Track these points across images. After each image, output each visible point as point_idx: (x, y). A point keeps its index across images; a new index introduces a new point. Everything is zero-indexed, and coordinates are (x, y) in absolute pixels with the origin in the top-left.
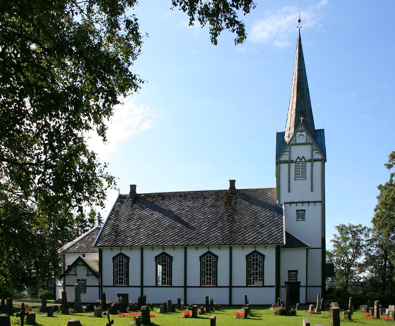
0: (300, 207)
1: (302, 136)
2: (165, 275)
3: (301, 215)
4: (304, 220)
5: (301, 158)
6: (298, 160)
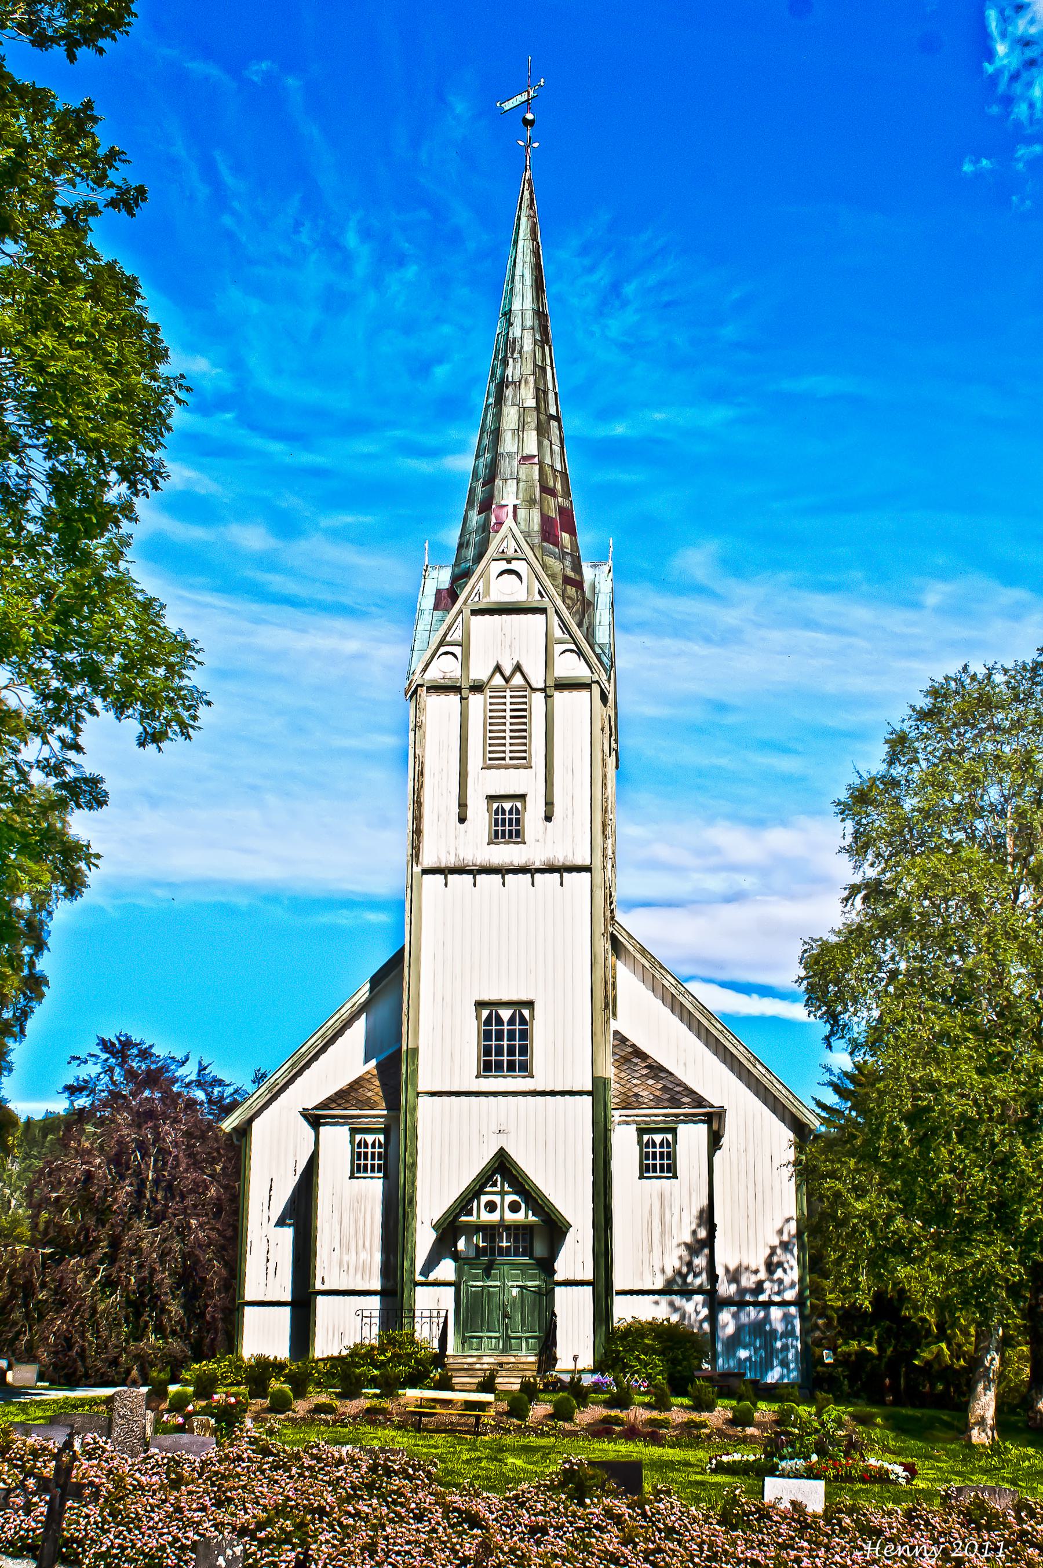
0: (506, 854)
1: (514, 577)
2: (359, 1153)
3: (370, 1150)
4: (675, 1177)
5: (507, 673)
6: (498, 680)
